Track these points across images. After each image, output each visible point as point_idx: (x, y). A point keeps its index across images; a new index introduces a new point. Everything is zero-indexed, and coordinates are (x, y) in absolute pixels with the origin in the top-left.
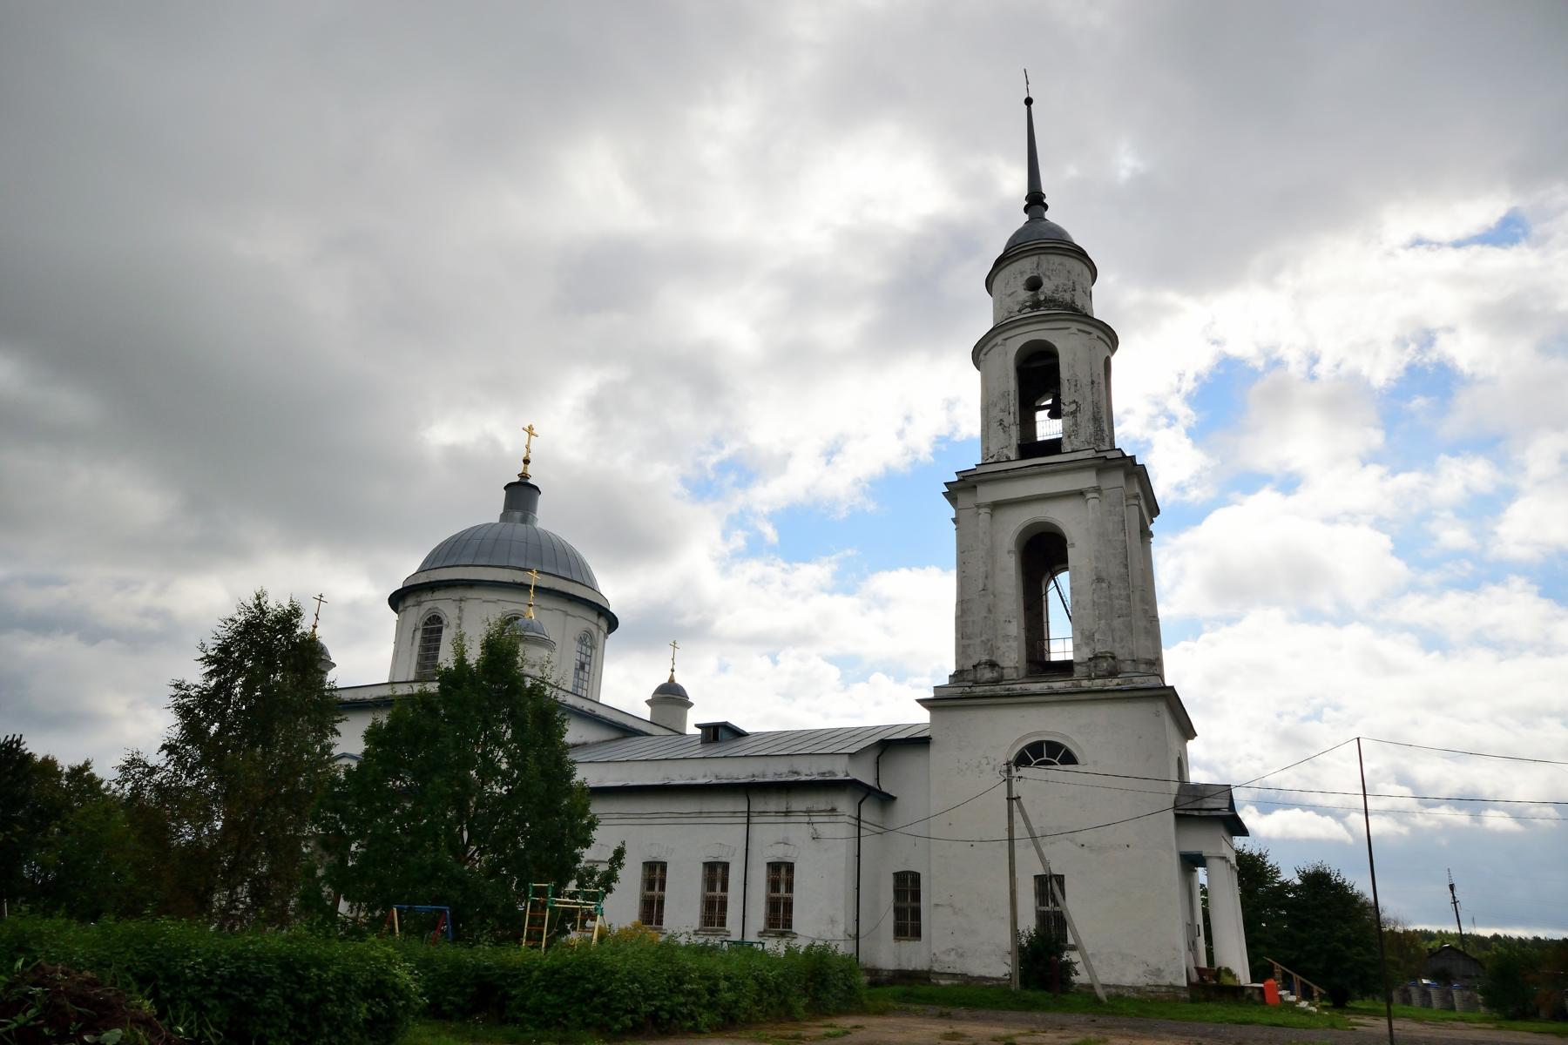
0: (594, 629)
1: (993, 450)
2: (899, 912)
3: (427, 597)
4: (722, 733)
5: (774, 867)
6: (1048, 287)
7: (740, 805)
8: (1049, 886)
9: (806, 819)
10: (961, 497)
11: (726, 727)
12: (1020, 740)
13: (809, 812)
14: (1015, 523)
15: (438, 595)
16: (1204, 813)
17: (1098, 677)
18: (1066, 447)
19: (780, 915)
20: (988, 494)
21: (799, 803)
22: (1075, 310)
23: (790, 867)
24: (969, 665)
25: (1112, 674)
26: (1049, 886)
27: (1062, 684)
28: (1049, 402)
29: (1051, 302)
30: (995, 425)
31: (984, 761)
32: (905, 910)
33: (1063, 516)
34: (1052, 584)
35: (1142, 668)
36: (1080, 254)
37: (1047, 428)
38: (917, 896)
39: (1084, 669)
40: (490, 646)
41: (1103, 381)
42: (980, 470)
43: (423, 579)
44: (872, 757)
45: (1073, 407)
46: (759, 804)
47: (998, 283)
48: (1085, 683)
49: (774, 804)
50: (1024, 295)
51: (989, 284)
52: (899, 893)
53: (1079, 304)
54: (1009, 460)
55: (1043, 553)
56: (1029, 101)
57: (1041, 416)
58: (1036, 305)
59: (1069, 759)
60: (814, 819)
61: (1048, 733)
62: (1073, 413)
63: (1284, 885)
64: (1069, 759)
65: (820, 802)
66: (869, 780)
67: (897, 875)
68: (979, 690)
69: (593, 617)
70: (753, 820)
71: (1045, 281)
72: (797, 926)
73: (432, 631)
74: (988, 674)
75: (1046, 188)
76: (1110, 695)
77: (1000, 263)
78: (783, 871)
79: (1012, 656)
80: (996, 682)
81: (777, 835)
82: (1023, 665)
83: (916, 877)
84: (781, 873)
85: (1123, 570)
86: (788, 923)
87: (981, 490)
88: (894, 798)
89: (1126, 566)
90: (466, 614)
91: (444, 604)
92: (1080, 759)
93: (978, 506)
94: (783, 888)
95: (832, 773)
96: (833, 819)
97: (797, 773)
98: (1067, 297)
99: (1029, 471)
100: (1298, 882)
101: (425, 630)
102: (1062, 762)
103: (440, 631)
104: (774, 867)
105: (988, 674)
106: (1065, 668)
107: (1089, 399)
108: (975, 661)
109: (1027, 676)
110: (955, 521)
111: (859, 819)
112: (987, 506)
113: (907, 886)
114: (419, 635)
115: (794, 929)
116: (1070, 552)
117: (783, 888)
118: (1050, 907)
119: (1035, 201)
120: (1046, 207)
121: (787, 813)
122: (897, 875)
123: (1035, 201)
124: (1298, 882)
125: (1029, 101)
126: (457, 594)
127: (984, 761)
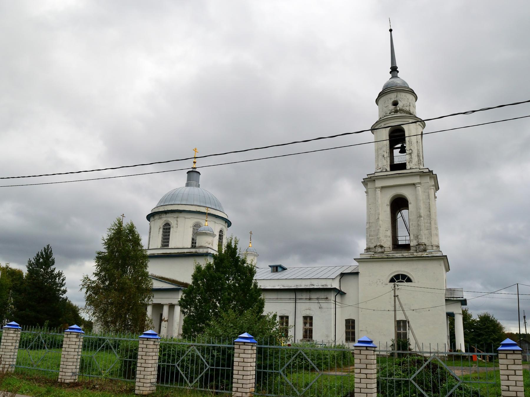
0: (224, 227)
1: (380, 166)
2: (347, 333)
3: (164, 216)
4: (279, 269)
5: (305, 318)
6: (400, 106)
7: (293, 296)
8: (402, 325)
9: (317, 301)
10: (370, 185)
11: (280, 266)
12: (392, 274)
13: (318, 299)
14: (390, 195)
15: (168, 215)
16: (455, 299)
17: (420, 251)
18: (408, 167)
19: (308, 334)
20: (379, 184)
21: (314, 296)
22: (410, 114)
23: (311, 318)
24: (372, 246)
25: (425, 250)
26: (402, 325)
27: (407, 254)
28: (399, 145)
29: (401, 110)
30: (381, 157)
31: (379, 281)
32: (349, 332)
33: (407, 193)
34: (399, 214)
35: (435, 248)
36: (412, 92)
37: (399, 157)
38: (353, 327)
39: (414, 248)
40: (229, 246)
41: (420, 141)
42: (377, 174)
43: (161, 209)
44: (338, 278)
45: (411, 151)
46: (299, 296)
47: (381, 101)
48: (415, 254)
49: (305, 296)
50: (392, 107)
51: (377, 101)
52: (347, 327)
53: (412, 111)
54: (386, 171)
55: (399, 204)
56: (391, 30)
57: (396, 152)
58: (396, 111)
59: (409, 280)
60: (320, 301)
61: (410, 274)
62: (410, 154)
63: (473, 321)
64: (409, 280)
65: (322, 295)
66: (338, 288)
67: (346, 320)
68: (377, 256)
69: (223, 223)
70: (297, 301)
71: (399, 102)
72: (314, 338)
73: (167, 229)
74: (380, 250)
75: (398, 64)
76: (424, 258)
77: (381, 95)
78: (308, 319)
79: (388, 243)
80: (383, 252)
81: (305, 307)
82: (391, 246)
83: (353, 321)
84: (308, 320)
85: (429, 213)
86: (311, 337)
87: (377, 181)
88: (345, 294)
89: (430, 212)
90: (179, 223)
91: (171, 219)
92: (413, 281)
93: (376, 188)
94: (284, 324)
95: (326, 285)
96: (327, 301)
97: (313, 285)
98: (407, 109)
99: (395, 175)
100: (478, 319)
101: (164, 229)
102: (407, 281)
103: (170, 229)
104: (305, 318)
105: (380, 250)
106: (407, 247)
107: (416, 148)
108: (375, 245)
109: (393, 250)
110: (366, 192)
111: (335, 301)
112: (379, 188)
113: (350, 324)
114: (161, 230)
115: (313, 339)
116: (410, 206)
117: (284, 324)
118: (402, 331)
119: (394, 70)
120: (398, 72)
121: (310, 299)
122: (346, 320)
123: (394, 70)
124: (478, 319)
125: (391, 30)
126: (176, 215)
127: (379, 281)
